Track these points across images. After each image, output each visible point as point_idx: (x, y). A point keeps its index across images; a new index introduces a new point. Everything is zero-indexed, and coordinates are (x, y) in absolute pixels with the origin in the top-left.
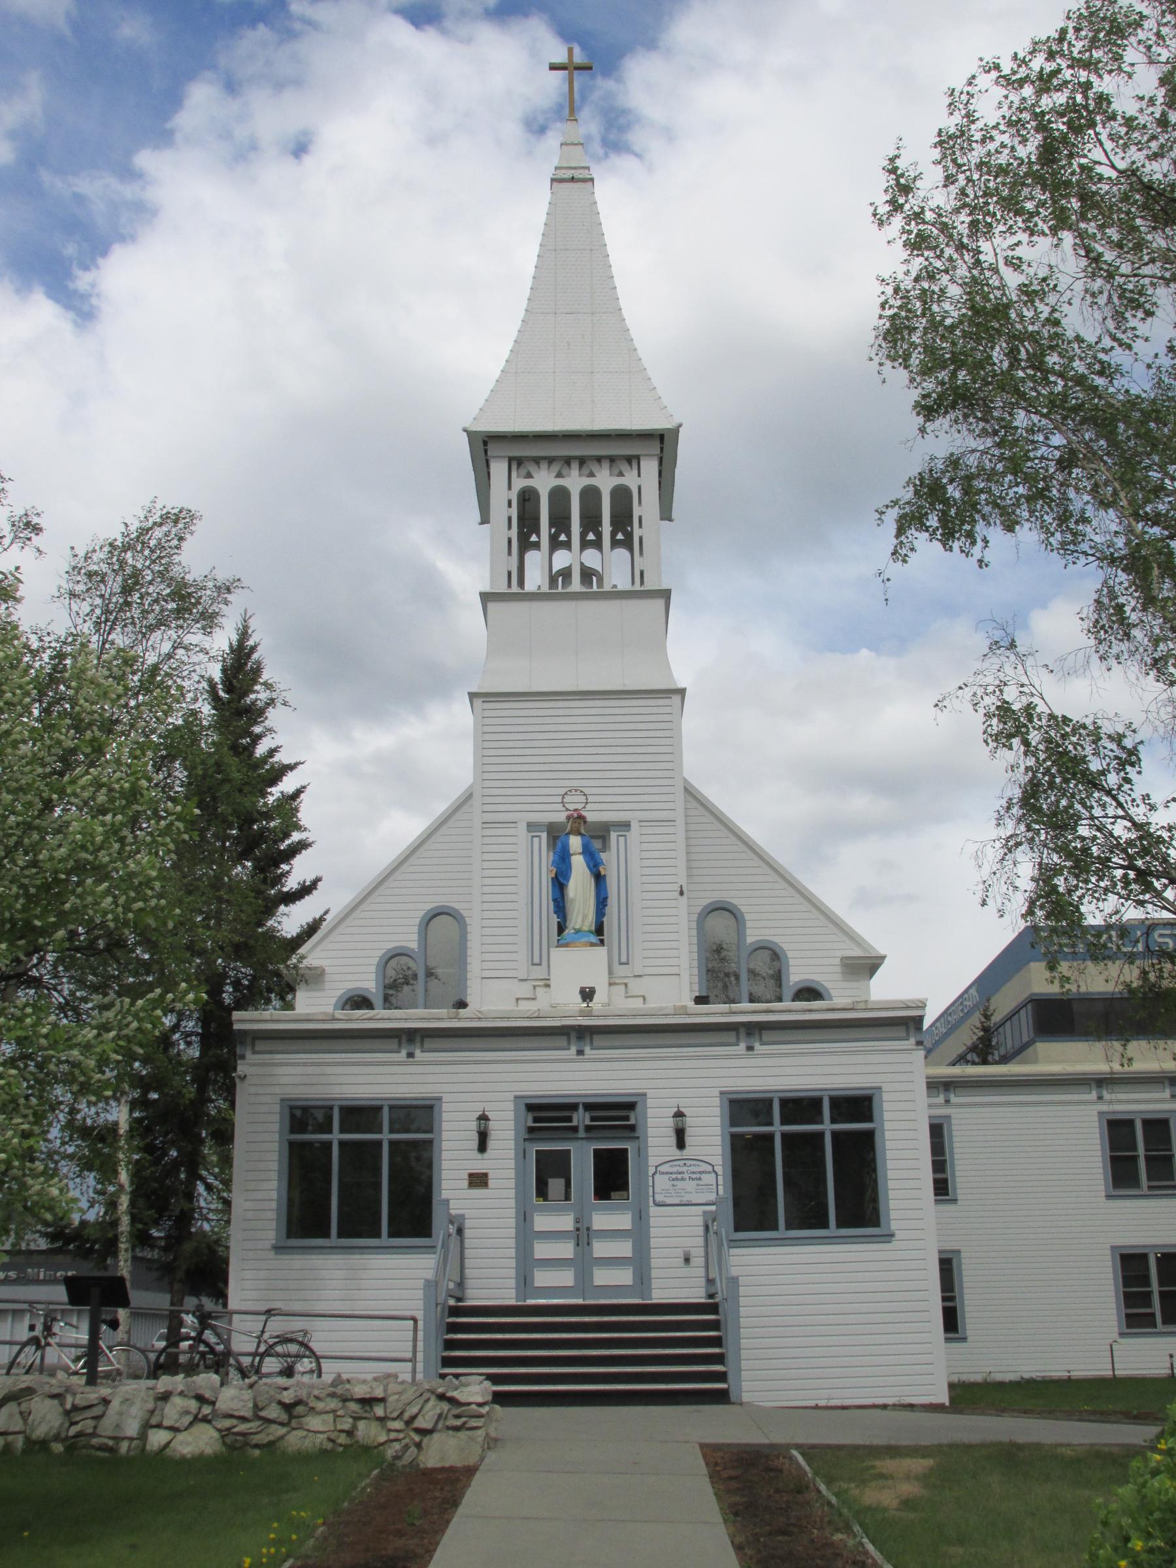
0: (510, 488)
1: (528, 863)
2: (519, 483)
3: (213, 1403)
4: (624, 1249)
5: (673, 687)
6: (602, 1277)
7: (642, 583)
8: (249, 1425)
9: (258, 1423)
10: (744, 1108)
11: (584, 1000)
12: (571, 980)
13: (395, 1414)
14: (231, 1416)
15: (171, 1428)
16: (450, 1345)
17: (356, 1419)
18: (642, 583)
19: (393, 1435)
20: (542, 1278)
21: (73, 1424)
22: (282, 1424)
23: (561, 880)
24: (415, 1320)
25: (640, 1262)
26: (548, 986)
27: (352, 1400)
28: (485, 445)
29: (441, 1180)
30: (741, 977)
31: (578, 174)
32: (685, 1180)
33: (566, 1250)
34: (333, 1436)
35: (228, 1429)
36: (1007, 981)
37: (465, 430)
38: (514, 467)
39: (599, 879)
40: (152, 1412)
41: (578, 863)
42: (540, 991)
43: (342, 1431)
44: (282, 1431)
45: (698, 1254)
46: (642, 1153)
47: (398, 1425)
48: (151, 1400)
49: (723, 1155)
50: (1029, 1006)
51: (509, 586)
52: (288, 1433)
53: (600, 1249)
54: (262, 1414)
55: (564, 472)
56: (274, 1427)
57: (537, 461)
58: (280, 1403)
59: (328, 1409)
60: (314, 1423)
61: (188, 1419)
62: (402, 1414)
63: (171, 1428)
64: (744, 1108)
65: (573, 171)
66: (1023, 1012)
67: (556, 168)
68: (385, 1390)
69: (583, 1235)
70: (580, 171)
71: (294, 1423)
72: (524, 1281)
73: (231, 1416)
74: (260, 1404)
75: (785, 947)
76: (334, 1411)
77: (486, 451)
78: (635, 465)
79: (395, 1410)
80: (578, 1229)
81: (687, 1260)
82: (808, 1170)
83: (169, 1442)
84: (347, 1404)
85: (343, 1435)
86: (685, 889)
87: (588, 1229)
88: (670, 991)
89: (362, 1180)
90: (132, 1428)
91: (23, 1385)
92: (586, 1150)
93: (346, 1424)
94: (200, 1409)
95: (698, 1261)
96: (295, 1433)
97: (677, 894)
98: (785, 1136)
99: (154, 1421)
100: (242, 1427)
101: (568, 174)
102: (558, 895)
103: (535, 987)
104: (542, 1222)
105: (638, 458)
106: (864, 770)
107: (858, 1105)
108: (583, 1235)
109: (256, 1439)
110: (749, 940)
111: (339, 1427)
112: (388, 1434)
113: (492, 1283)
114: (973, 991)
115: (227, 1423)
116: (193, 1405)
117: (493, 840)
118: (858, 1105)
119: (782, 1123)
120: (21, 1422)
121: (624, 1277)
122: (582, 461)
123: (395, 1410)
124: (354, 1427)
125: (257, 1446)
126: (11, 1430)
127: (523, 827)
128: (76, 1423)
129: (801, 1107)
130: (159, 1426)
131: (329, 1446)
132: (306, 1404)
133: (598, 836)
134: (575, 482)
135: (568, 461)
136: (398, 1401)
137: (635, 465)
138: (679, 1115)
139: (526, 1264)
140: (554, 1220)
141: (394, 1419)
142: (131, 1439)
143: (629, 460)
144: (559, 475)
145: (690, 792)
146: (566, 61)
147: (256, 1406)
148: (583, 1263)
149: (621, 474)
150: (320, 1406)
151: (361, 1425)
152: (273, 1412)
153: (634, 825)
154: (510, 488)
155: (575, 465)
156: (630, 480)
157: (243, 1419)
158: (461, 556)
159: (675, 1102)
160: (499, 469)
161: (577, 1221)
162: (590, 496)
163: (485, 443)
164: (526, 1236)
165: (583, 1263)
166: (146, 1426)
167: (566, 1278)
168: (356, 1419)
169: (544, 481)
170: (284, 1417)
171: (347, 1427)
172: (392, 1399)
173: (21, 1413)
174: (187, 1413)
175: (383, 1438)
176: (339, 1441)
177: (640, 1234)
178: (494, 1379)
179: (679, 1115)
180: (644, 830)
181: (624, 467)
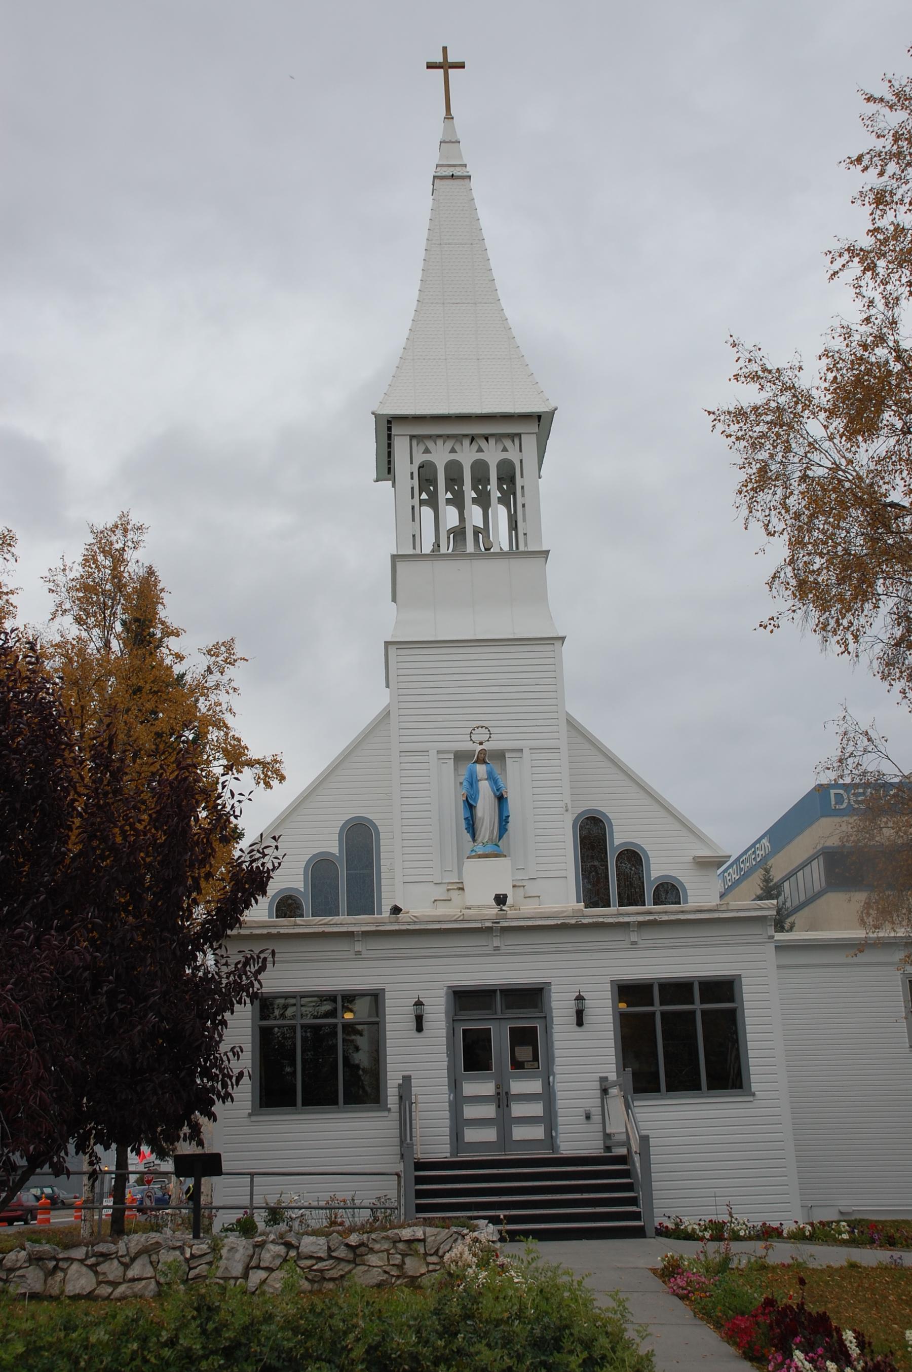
0: (411, 463)
1: (443, 787)
2: (419, 458)
3: (297, 1248)
4: (537, 1109)
5: (555, 635)
6: (520, 1133)
7: (526, 545)
8: (324, 1263)
9: (331, 1261)
10: (629, 992)
11: (498, 904)
12: (483, 885)
13: (433, 1251)
14: (311, 1257)
15: (266, 1269)
16: (419, 1194)
17: (404, 1255)
18: (526, 545)
19: (431, 1267)
20: (471, 1135)
21: (190, 1269)
22: (349, 1262)
23: (471, 802)
24: (398, 1175)
25: (549, 1120)
26: (463, 889)
27: (400, 1241)
28: (388, 426)
29: (386, 1055)
30: (608, 869)
31: (458, 172)
32: (585, 1054)
33: (489, 1111)
34: (387, 1269)
35: (310, 1267)
36: (799, 834)
37: (373, 413)
38: (414, 443)
39: (501, 799)
40: (252, 1257)
41: (485, 787)
42: (455, 895)
43: (393, 1265)
44: (348, 1267)
45: (596, 1111)
46: (547, 1030)
47: (434, 1259)
48: (251, 1247)
49: (614, 1031)
50: (821, 859)
51: (414, 548)
52: (354, 1268)
53: (518, 1110)
54: (334, 1254)
55: (457, 448)
56: (343, 1265)
57: (434, 438)
58: (347, 1245)
59: (382, 1249)
60: (373, 1259)
61: (278, 1262)
62: (437, 1250)
63: (266, 1269)
64: (629, 992)
65: (452, 169)
66: (815, 863)
67: (437, 166)
68: (424, 1234)
69: (503, 1099)
70: (458, 169)
71: (358, 1260)
72: (457, 1136)
73: (311, 1257)
74: (333, 1247)
75: (610, 816)
76: (387, 1250)
77: (389, 429)
78: (517, 441)
79: (432, 1248)
80: (498, 1094)
81: (588, 1117)
82: (684, 1041)
83: (266, 1279)
84: (397, 1244)
85: (395, 1268)
86: (569, 806)
87: (507, 1093)
88: (557, 890)
89: (321, 1062)
90: (237, 1269)
91: (153, 1241)
92: (498, 1029)
93: (397, 1259)
94: (288, 1253)
95: (596, 1118)
96: (359, 1268)
97: (563, 810)
98: (663, 1014)
99: (253, 1264)
100: (320, 1265)
101: (448, 172)
102: (469, 815)
103: (448, 890)
104: (471, 1088)
105: (519, 435)
106: (709, 691)
107: (723, 990)
108: (503, 1099)
109: (328, 1275)
110: (617, 842)
111: (391, 1263)
112: (428, 1266)
113: (435, 1142)
114: (765, 841)
115: (309, 1262)
116: (281, 1249)
117: (409, 766)
118: (723, 990)
119: (661, 1004)
120: (151, 1269)
121: (537, 1132)
122: (473, 439)
123: (432, 1248)
124: (404, 1263)
125: (332, 1279)
126: (145, 1276)
127: (433, 753)
128: (195, 1268)
129: (677, 990)
130: (258, 1267)
131: (385, 1277)
132: (367, 1246)
133: (492, 758)
134: (467, 456)
135: (458, 438)
136: (434, 1241)
137: (517, 441)
138: (580, 998)
139: (458, 1124)
140: (480, 1086)
141: (431, 1255)
142: (237, 1278)
143: (512, 437)
144: (453, 451)
145: (572, 724)
146: (442, 61)
147: (329, 1248)
148: (504, 1122)
149: (505, 450)
150: (377, 1247)
151: (408, 1260)
152: (342, 1253)
153: (526, 752)
154: (411, 463)
155: (466, 442)
156: (513, 455)
157: (320, 1259)
158: (369, 519)
159: (577, 988)
160: (401, 447)
161: (497, 1087)
162: (480, 469)
163: (389, 422)
164: (458, 1102)
165: (504, 1122)
166: (247, 1269)
167: (490, 1135)
168: (404, 1255)
169: (440, 456)
170: (351, 1256)
171: (397, 1262)
172: (429, 1240)
173: (151, 1262)
174: (279, 1256)
175: (423, 1270)
176: (392, 1273)
177: (548, 1097)
178: (494, 1220)
179: (580, 998)
180: (535, 756)
181: (508, 443)
